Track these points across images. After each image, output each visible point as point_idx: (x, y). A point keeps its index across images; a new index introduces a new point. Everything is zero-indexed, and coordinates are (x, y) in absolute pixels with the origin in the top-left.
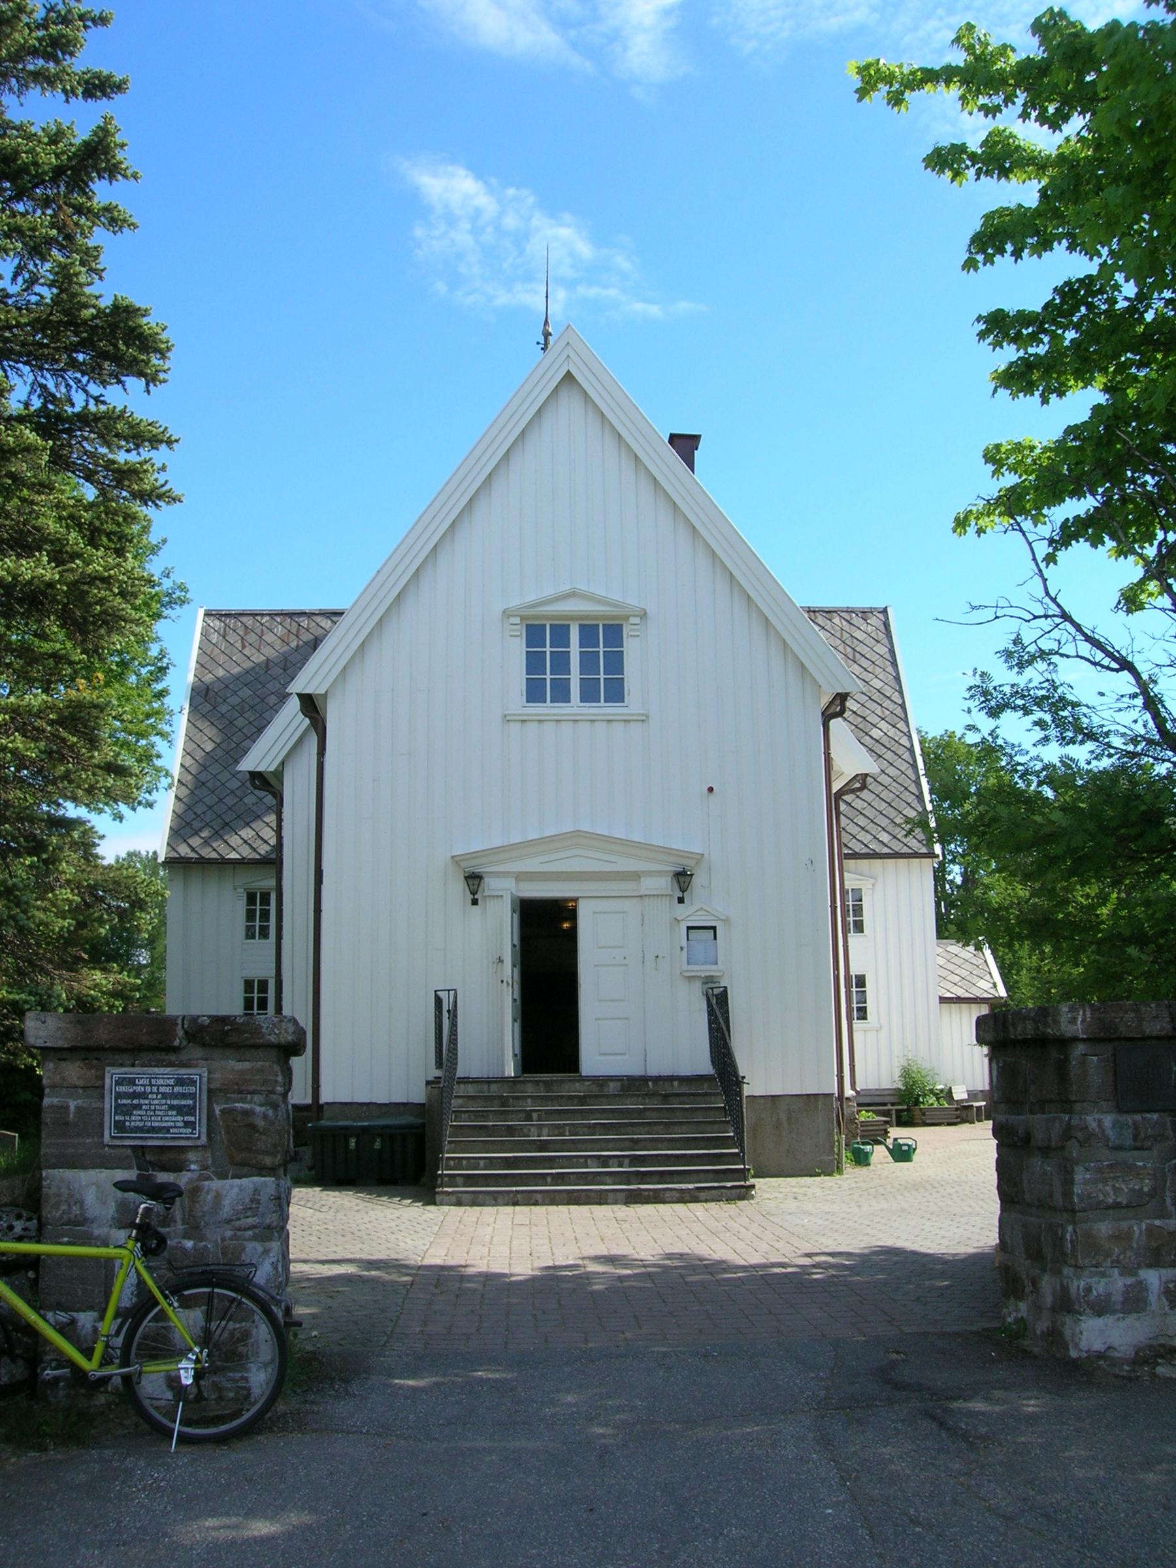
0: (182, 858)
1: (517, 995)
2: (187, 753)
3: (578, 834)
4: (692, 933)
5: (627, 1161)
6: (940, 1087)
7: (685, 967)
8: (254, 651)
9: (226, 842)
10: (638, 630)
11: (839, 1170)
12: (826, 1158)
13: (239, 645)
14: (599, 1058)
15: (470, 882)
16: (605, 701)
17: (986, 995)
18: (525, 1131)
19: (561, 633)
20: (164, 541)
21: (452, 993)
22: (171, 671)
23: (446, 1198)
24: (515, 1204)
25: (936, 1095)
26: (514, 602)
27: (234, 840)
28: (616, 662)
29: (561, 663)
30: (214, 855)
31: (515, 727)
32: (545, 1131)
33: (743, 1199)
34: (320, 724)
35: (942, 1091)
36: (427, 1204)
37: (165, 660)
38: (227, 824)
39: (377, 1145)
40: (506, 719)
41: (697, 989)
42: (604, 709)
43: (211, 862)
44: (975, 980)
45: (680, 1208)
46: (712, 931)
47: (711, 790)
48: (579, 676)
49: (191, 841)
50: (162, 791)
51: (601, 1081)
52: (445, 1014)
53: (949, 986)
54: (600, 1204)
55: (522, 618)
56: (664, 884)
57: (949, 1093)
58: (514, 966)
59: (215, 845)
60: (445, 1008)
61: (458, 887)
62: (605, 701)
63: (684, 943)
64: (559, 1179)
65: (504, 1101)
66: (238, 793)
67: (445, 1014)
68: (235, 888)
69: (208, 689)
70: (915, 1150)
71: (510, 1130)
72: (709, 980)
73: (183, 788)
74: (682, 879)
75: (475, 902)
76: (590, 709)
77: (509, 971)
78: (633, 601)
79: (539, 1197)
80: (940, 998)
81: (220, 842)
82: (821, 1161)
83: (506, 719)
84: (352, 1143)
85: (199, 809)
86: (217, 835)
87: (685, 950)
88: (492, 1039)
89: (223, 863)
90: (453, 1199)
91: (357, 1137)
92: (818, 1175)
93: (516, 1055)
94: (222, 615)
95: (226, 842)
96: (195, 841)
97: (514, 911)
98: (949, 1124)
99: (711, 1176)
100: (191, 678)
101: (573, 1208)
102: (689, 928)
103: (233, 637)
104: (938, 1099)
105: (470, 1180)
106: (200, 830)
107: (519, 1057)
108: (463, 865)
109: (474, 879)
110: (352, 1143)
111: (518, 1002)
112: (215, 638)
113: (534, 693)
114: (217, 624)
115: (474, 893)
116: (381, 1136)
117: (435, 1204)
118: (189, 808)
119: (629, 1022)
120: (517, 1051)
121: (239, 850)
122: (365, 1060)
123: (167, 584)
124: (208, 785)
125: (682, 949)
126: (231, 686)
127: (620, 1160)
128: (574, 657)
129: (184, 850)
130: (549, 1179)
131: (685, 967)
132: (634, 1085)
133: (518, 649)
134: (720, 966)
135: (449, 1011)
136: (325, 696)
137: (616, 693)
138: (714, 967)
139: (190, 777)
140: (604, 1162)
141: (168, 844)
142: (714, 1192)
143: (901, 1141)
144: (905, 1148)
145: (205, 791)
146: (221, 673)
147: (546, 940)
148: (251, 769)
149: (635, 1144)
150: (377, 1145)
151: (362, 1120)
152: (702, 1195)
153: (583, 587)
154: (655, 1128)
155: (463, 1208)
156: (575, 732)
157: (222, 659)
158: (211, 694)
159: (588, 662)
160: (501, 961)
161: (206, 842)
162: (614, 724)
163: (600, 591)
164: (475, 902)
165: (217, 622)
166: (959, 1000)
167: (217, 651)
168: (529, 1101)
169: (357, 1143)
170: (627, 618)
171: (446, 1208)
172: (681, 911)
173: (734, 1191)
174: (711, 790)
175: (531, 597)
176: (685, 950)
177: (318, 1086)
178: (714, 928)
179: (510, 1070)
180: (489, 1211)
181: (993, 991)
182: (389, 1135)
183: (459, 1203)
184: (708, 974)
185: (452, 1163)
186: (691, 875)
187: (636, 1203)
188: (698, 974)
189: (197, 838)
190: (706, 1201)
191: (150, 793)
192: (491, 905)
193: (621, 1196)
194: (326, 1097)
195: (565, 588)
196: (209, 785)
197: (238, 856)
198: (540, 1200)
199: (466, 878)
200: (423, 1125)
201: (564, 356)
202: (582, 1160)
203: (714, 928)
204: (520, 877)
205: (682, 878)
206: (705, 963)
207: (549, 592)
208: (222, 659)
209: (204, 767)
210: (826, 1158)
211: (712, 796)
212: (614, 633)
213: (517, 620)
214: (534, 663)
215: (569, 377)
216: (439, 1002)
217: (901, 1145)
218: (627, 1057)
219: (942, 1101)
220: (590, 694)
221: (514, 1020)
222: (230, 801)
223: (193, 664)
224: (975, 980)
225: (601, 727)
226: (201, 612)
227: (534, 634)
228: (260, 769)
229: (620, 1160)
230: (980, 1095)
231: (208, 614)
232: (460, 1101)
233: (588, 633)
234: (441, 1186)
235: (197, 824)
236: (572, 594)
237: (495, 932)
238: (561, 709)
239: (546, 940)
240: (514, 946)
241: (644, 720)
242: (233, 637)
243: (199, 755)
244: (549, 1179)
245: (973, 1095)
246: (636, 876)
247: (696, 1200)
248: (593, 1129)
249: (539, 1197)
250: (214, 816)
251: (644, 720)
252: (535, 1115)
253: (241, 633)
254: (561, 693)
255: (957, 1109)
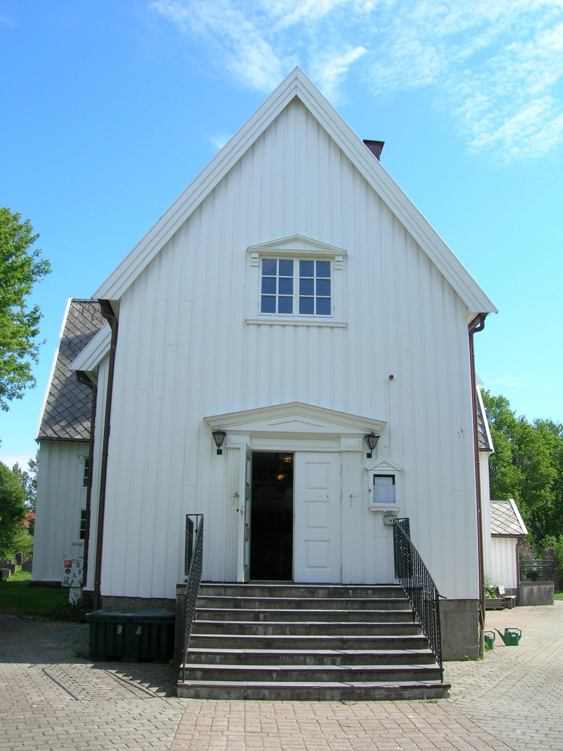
0: (48, 437)
1: (248, 521)
2: (56, 377)
3: (296, 405)
4: (378, 480)
5: (339, 660)
6: (491, 587)
7: (372, 504)
8: (98, 322)
9: (74, 429)
10: (341, 265)
11: (481, 656)
12: (471, 647)
13: (90, 319)
14: (307, 569)
15: (217, 437)
16: (317, 314)
17: (516, 533)
18: (254, 629)
19: (287, 266)
20: (38, 236)
21: (199, 517)
22: (41, 320)
23: (186, 691)
24: (246, 698)
25: (489, 591)
26: (255, 242)
27: (80, 428)
28: (325, 287)
29: (287, 286)
30: (67, 436)
31: (253, 329)
32: (270, 630)
33: (440, 697)
34: (114, 323)
35: (493, 588)
36: (168, 696)
37: (38, 313)
38: (76, 419)
39: (139, 632)
40: (247, 323)
41: (380, 518)
42: (316, 318)
43: (66, 440)
44: (509, 524)
45: (387, 704)
46: (391, 479)
47: (391, 377)
48: (298, 296)
49: (54, 428)
50: (28, 388)
51: (312, 590)
52: (193, 536)
53: (494, 527)
54: (319, 700)
55: (261, 254)
56: (358, 443)
57: (497, 590)
58: (247, 499)
59: (68, 430)
60: (195, 528)
61: (208, 441)
62: (317, 314)
63: (371, 486)
64: (284, 675)
65: (237, 603)
66: (84, 401)
67: (193, 536)
68: (79, 456)
69: (70, 342)
70: (520, 637)
71: (242, 629)
72: (388, 514)
73: (52, 397)
74: (371, 440)
75: (219, 452)
76: (306, 318)
77: (243, 503)
78: (337, 244)
79: (266, 692)
80: (492, 534)
81: (71, 429)
82: (468, 649)
83: (247, 323)
84: (120, 629)
85: (60, 409)
86: (70, 424)
87: (372, 491)
88: (228, 552)
89: (72, 441)
90: (192, 692)
91: (124, 624)
92: (466, 660)
93: (246, 566)
94: (81, 302)
95: (74, 429)
96: (57, 428)
97: (248, 459)
98: (497, 609)
99: (411, 675)
100: (61, 335)
101: (297, 703)
102: (375, 476)
103: (86, 314)
104: (491, 594)
105: (208, 674)
106: (60, 421)
107: (248, 567)
108: (213, 424)
109: (219, 436)
110: (120, 629)
111: (249, 526)
112: (76, 314)
113: (267, 305)
114: (78, 307)
115: (219, 445)
116: (141, 624)
117: (176, 695)
118: (55, 408)
119: (333, 542)
120: (247, 563)
121: (82, 434)
122: (135, 567)
123: (37, 260)
124: (67, 396)
125: (370, 490)
126: (84, 341)
127: (333, 659)
128: (296, 283)
129: (50, 433)
130: (275, 675)
131: (372, 504)
132: (339, 592)
133: (256, 276)
134: (397, 504)
135: (196, 531)
136: (118, 302)
137: (325, 308)
138: (392, 505)
139: (56, 391)
140: (320, 659)
141: (41, 429)
142: (416, 691)
143: (511, 631)
144: (514, 636)
145: (64, 399)
146: (78, 333)
147: (271, 482)
148: (77, 369)
149: (344, 644)
150: (139, 632)
151: (129, 610)
152: (406, 693)
153: (302, 233)
154: (359, 630)
155: (200, 701)
156: (295, 332)
157: (80, 326)
158: (72, 345)
159: (306, 286)
160: (237, 496)
161: (63, 429)
162: (323, 329)
163: (315, 237)
164: (219, 452)
165: (79, 306)
166: (500, 535)
167: (77, 322)
168: (257, 603)
169: (123, 629)
170: (333, 257)
171: (185, 701)
172: (369, 463)
173: (433, 690)
174: (391, 377)
175: (267, 239)
176: (372, 491)
177: (100, 583)
178: (393, 476)
179: (241, 577)
180: (223, 704)
181: (519, 530)
182: (148, 624)
183: (197, 696)
184: (388, 510)
185: (193, 657)
186: (378, 437)
187: (349, 699)
188: (381, 509)
189: (58, 426)
190: (409, 699)
191: (20, 389)
192: (232, 455)
193: (337, 693)
194: (104, 591)
195: (290, 234)
196: (67, 396)
197: (81, 438)
198: (267, 695)
199: (214, 434)
200: (173, 618)
201: (293, 86)
202: (302, 658)
203: (393, 476)
204: (253, 435)
205: (371, 439)
206: (387, 501)
207: (279, 236)
208: (80, 326)
209: (65, 386)
210: (471, 647)
211: (392, 383)
212: (324, 267)
213: (257, 255)
214: (267, 285)
215: (296, 100)
216: (189, 524)
217: (511, 634)
218: (327, 569)
219: (493, 595)
220: (306, 308)
221: (246, 540)
222: (78, 405)
223: (63, 328)
224: (509, 524)
225: (314, 331)
226: (70, 300)
227: (268, 266)
228: (83, 369)
229: (333, 659)
230: (511, 591)
231: (74, 301)
232: (203, 602)
233: (306, 267)
234: (183, 679)
235: (58, 418)
236: (296, 239)
237: (234, 473)
238: (285, 317)
239: (271, 482)
240: (247, 484)
241: (345, 327)
242: (86, 314)
243: (63, 379)
244: (275, 675)
245: (508, 591)
246: (337, 437)
247: (400, 697)
248: (308, 630)
249: (266, 692)
250: (69, 414)
251: (345, 327)
252: (261, 616)
253: (92, 312)
254: (286, 307)
255: (503, 601)
